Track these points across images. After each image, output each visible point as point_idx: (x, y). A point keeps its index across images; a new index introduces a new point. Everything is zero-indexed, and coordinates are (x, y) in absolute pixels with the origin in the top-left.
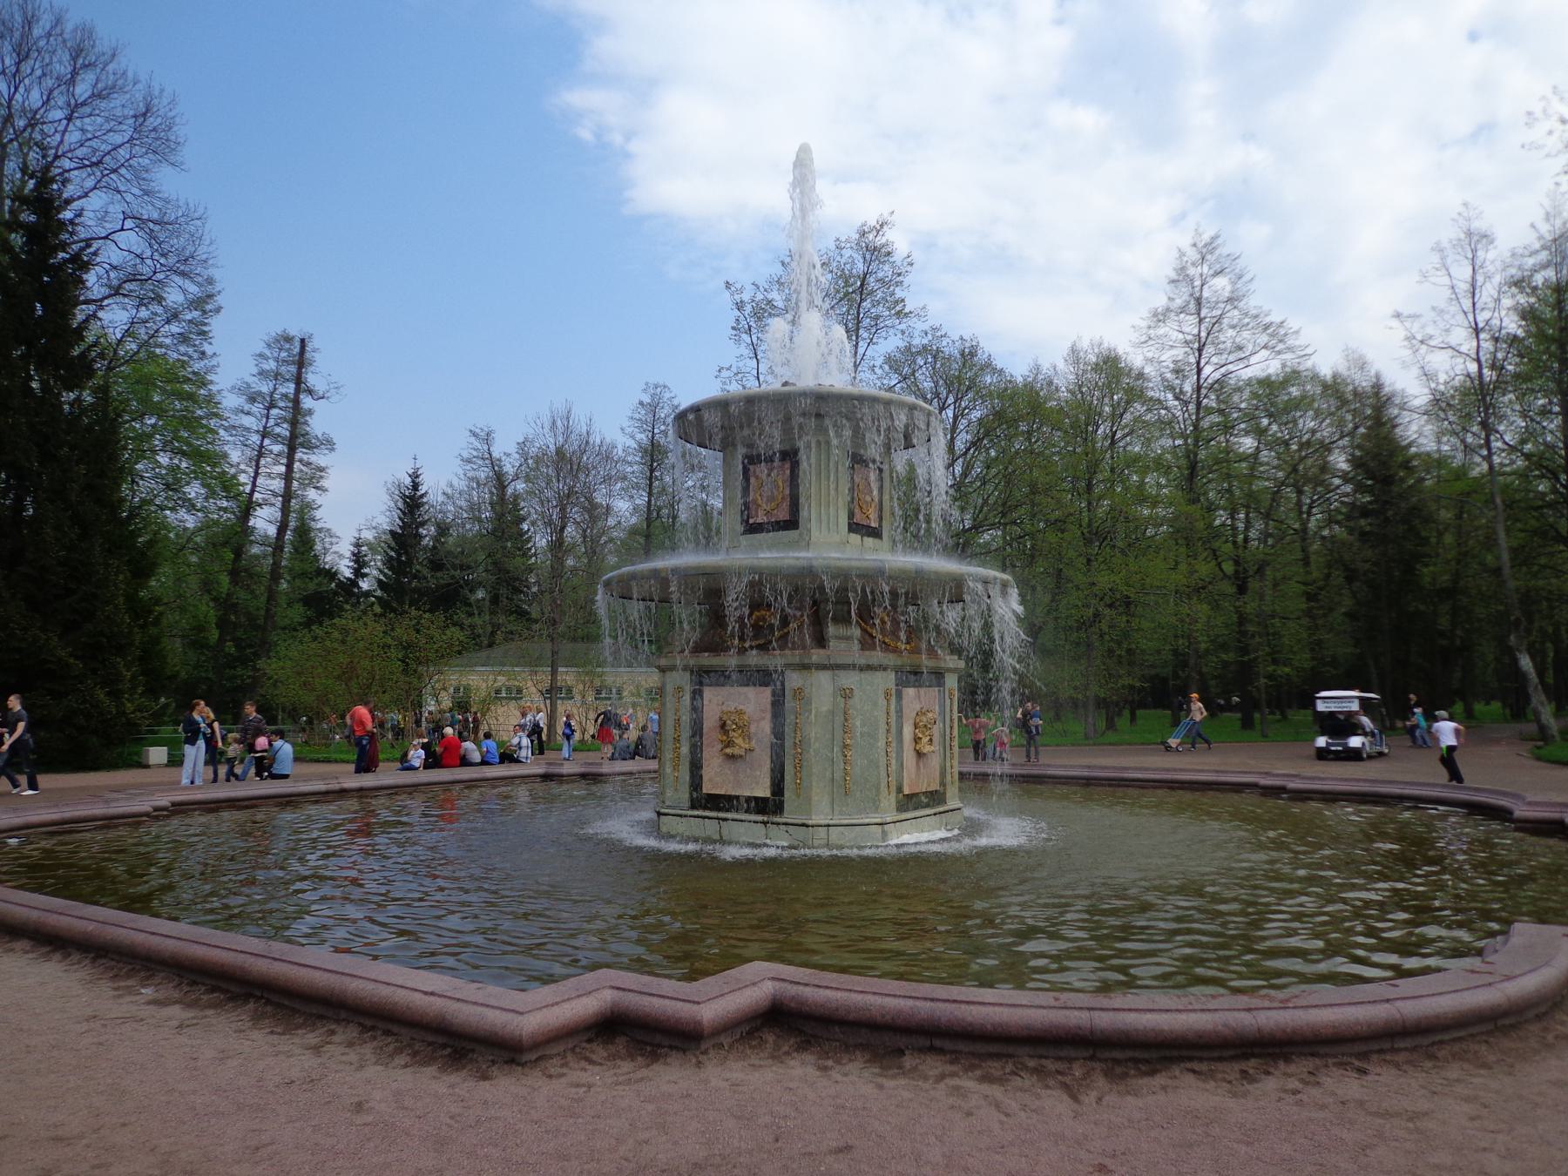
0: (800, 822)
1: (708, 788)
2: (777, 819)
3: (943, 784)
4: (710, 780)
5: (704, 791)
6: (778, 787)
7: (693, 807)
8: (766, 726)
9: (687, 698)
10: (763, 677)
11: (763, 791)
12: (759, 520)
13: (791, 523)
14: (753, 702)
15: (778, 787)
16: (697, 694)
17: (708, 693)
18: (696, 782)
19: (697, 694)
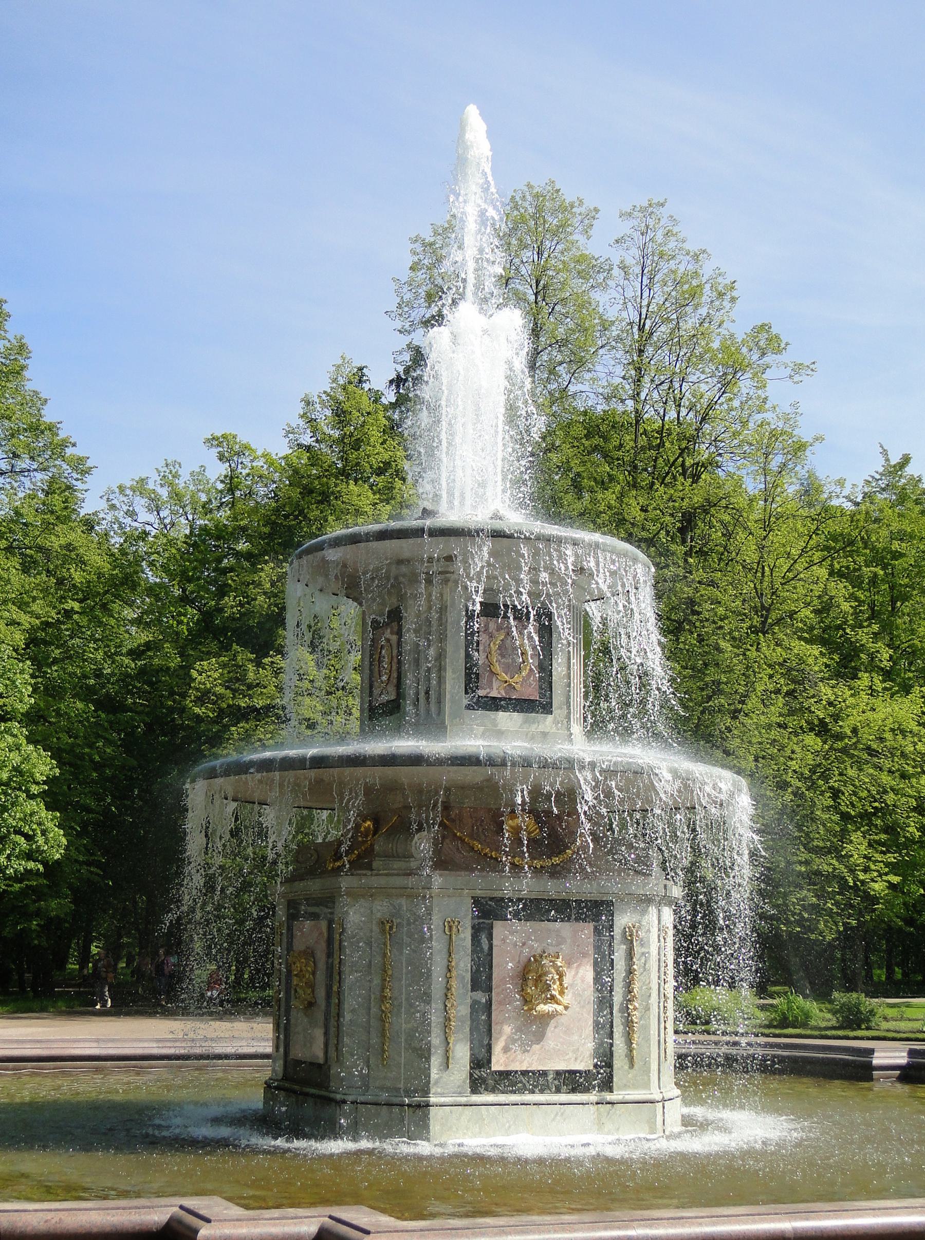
2: (609, 1097)
3: (290, 929)
6: (606, 1059)
7: (474, 1090)
9: (466, 935)
11: (584, 1062)
12: (494, 694)
15: (606, 1059)
17: (499, 929)
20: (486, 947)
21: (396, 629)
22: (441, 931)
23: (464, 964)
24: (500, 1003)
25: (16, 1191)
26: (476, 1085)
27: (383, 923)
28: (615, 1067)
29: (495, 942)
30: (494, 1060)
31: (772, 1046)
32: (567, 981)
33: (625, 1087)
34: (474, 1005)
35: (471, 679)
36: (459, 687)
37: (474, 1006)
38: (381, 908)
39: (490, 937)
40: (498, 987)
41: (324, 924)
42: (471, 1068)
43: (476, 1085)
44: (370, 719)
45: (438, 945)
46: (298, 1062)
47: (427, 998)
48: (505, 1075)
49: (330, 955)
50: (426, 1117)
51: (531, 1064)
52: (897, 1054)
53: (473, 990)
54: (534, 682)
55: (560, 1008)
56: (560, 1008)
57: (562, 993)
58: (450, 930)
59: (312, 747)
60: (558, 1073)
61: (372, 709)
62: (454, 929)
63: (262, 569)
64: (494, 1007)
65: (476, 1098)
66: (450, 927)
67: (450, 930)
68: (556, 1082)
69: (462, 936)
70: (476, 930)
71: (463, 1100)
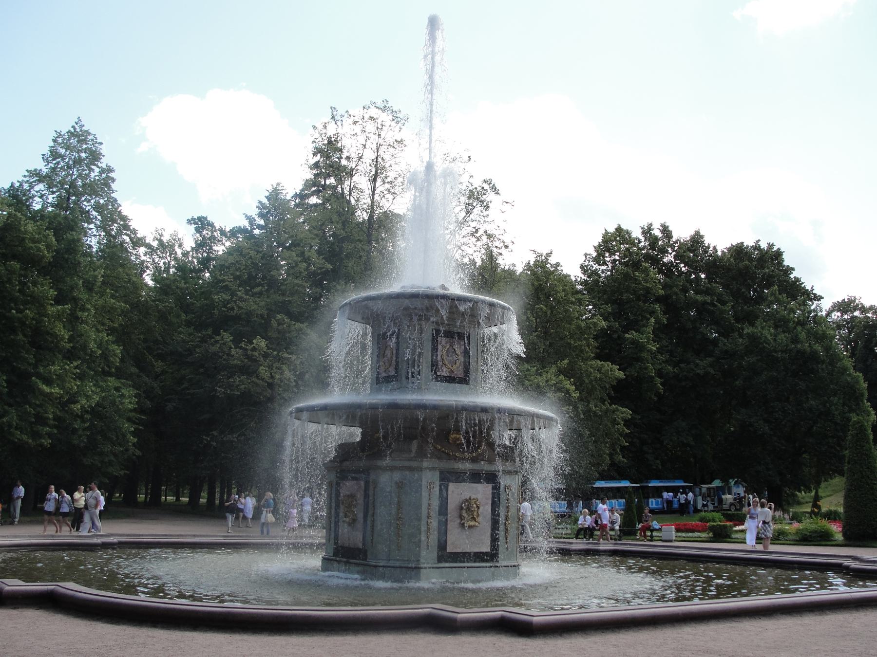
1: (450, 549)
5: (448, 550)
7: (439, 561)
8: (489, 508)
9: (437, 489)
10: (491, 478)
11: (486, 548)
13: (464, 380)
14: (482, 492)
16: (444, 488)
17: (452, 486)
18: (442, 546)
19: (444, 488)
23: (436, 503)
24: (451, 521)
25: (433, 583)
26: (440, 559)
29: (449, 493)
30: (448, 547)
31: (558, 542)
33: (504, 560)
34: (439, 522)
35: (434, 365)
38: (397, 476)
39: (447, 490)
41: (362, 483)
43: (440, 559)
45: (425, 494)
47: (419, 519)
50: (420, 572)
51: (463, 550)
52: (697, 534)
53: (439, 515)
54: (461, 368)
55: (477, 524)
56: (477, 524)
57: (478, 516)
59: (301, 403)
61: (377, 378)
63: (667, 256)
69: (435, 489)
70: (441, 490)
71: (435, 566)
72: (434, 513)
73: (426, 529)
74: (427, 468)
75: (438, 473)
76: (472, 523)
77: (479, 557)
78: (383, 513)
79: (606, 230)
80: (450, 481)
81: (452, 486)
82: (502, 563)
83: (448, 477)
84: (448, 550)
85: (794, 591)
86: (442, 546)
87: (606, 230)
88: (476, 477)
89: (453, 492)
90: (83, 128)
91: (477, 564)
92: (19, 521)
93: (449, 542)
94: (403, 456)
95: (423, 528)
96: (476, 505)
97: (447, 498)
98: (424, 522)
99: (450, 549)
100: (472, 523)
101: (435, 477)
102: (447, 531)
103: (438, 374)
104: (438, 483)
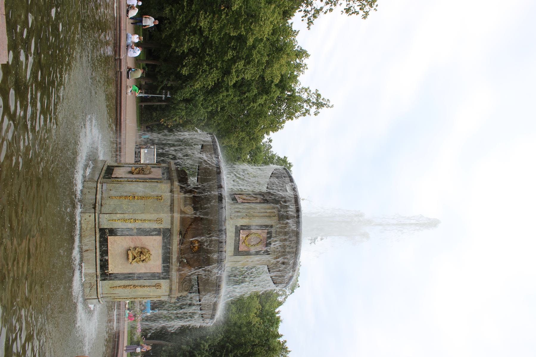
0: (145, 289)
1: (110, 239)
2: (99, 279)
3: (159, 167)
4: (115, 241)
5: (109, 237)
8: (143, 271)
9: (157, 226)
10: (166, 273)
11: (112, 269)
16: (158, 232)
17: (159, 238)
18: (112, 232)
20: (153, 233)
21: (262, 201)
22: (158, 217)
23: (147, 225)
24: (132, 239)
27: (161, 196)
28: (110, 281)
29: (154, 237)
32: (141, 263)
36: (243, 223)
37: (131, 229)
38: (167, 195)
40: (138, 238)
41: (161, 177)
42: (109, 229)
44: (119, 333)
45: (154, 216)
46: (113, 170)
48: (106, 240)
49: (150, 179)
51: (110, 250)
56: (130, 260)
58: (157, 286)
60: (107, 261)
62: (158, 287)
64: (131, 237)
65: (97, 231)
66: (158, 286)
67: (157, 286)
68: (104, 260)
70: (155, 230)
72: (138, 225)
73: (126, 218)
74: (172, 218)
75: (170, 227)
76: (131, 257)
77: (104, 265)
78: (140, 188)
79: (290, 351)
80: (164, 236)
81: (159, 238)
82: (100, 283)
83: (166, 234)
84: (109, 237)
85: (184, 308)
86: (112, 232)
87: (290, 351)
88: (166, 259)
89: (155, 240)
90: (318, 92)
91: (98, 262)
92: (144, 29)
93: (116, 238)
94: (181, 201)
95: (126, 216)
96: (146, 259)
97: (150, 235)
98: (131, 216)
99: (110, 239)
100: (131, 257)
101: (166, 225)
102: (124, 235)
103: (241, 231)
104: (161, 226)
